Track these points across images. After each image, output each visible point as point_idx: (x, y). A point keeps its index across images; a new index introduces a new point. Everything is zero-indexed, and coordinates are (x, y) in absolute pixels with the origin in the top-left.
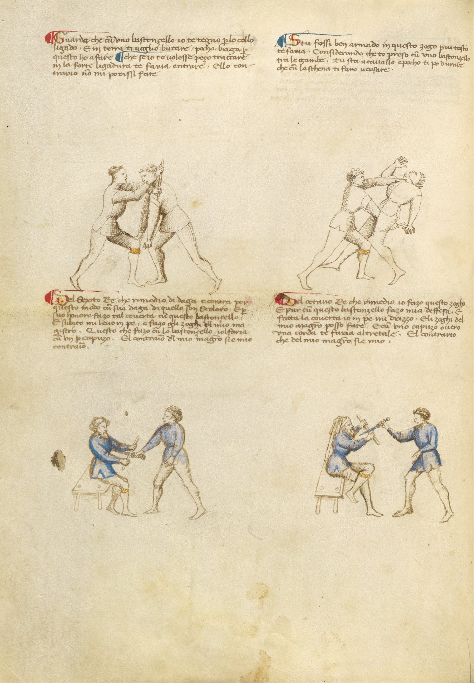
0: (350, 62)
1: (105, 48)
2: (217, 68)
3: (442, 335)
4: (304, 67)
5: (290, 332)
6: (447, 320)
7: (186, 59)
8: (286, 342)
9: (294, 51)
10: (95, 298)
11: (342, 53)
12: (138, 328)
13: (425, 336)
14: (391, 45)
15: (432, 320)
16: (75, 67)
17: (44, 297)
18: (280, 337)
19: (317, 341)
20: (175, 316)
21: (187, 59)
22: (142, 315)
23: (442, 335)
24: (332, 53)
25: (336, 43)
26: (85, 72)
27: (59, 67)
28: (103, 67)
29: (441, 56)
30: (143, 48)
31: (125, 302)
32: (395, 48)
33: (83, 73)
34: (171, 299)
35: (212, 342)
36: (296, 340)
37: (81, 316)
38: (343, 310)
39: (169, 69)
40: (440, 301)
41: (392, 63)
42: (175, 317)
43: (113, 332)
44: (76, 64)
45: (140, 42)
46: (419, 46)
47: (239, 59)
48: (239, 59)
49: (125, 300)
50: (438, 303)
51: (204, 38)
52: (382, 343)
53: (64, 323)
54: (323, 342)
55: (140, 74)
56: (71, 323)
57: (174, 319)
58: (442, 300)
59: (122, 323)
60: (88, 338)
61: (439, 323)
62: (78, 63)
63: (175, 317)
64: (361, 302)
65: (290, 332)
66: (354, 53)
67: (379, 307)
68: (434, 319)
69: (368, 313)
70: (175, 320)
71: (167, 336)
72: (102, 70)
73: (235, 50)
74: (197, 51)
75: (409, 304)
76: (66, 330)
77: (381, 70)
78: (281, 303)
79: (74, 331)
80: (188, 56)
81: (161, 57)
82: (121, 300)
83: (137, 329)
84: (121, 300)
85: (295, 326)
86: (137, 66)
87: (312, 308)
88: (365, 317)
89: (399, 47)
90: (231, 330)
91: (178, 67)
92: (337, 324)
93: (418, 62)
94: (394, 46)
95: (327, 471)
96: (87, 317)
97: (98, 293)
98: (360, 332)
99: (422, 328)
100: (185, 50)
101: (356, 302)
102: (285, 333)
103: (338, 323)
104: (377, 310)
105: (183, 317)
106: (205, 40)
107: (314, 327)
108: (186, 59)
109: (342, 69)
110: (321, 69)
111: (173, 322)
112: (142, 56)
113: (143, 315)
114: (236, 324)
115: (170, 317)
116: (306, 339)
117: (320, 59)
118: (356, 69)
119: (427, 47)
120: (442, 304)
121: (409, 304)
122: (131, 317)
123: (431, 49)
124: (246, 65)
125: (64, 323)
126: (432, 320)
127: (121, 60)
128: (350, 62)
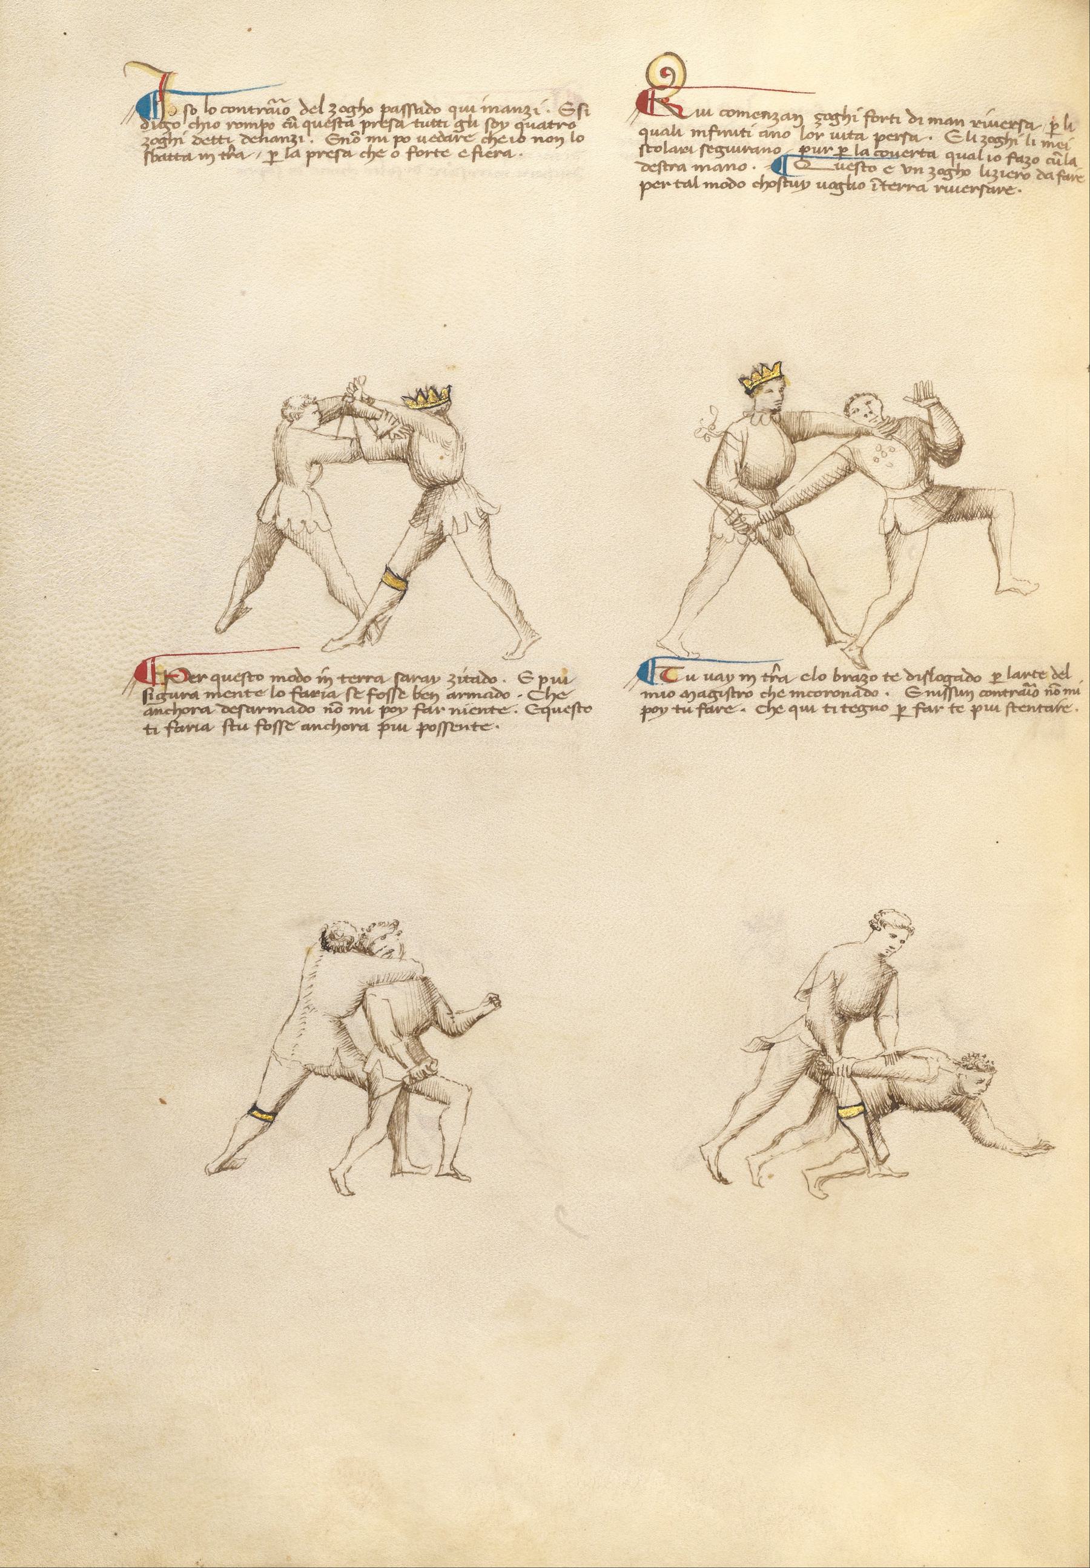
0: (228, 728)
2: (526, 683)
6: (170, 143)
8: (379, 156)
9: (382, 138)
10: (420, 121)
11: (477, 712)
12: (416, 148)
15: (975, 141)
16: (258, 730)
17: (635, 101)
20: (958, 155)
22: (909, 150)
25: (415, 694)
26: (329, 707)
27: (752, 679)
29: (155, 158)
33: (326, 709)
34: (914, 117)
35: (839, 192)
37: (810, 136)
42: (959, 157)
43: (258, 679)
50: (571, 710)
51: (856, 705)
55: (169, 728)
57: (957, 161)
58: (578, 703)
61: (991, 146)
63: (959, 157)
66: (421, 109)
68: (979, 139)
70: (959, 165)
79: (307, 679)
80: (285, 724)
83: (413, 149)
88: (768, 129)
89: (805, 712)
90: (262, 722)
91: (1029, 710)
92: (278, 724)
93: (654, 709)
102: (734, 165)
103: (281, 722)
105: (388, 124)
106: (859, 708)
107: (725, 152)
108: (281, 729)
110: (357, 680)
111: (955, 167)
114: (320, 127)
115: (947, 157)
120: (863, 171)
123: (866, 713)
124: (819, 187)
127: (649, 110)
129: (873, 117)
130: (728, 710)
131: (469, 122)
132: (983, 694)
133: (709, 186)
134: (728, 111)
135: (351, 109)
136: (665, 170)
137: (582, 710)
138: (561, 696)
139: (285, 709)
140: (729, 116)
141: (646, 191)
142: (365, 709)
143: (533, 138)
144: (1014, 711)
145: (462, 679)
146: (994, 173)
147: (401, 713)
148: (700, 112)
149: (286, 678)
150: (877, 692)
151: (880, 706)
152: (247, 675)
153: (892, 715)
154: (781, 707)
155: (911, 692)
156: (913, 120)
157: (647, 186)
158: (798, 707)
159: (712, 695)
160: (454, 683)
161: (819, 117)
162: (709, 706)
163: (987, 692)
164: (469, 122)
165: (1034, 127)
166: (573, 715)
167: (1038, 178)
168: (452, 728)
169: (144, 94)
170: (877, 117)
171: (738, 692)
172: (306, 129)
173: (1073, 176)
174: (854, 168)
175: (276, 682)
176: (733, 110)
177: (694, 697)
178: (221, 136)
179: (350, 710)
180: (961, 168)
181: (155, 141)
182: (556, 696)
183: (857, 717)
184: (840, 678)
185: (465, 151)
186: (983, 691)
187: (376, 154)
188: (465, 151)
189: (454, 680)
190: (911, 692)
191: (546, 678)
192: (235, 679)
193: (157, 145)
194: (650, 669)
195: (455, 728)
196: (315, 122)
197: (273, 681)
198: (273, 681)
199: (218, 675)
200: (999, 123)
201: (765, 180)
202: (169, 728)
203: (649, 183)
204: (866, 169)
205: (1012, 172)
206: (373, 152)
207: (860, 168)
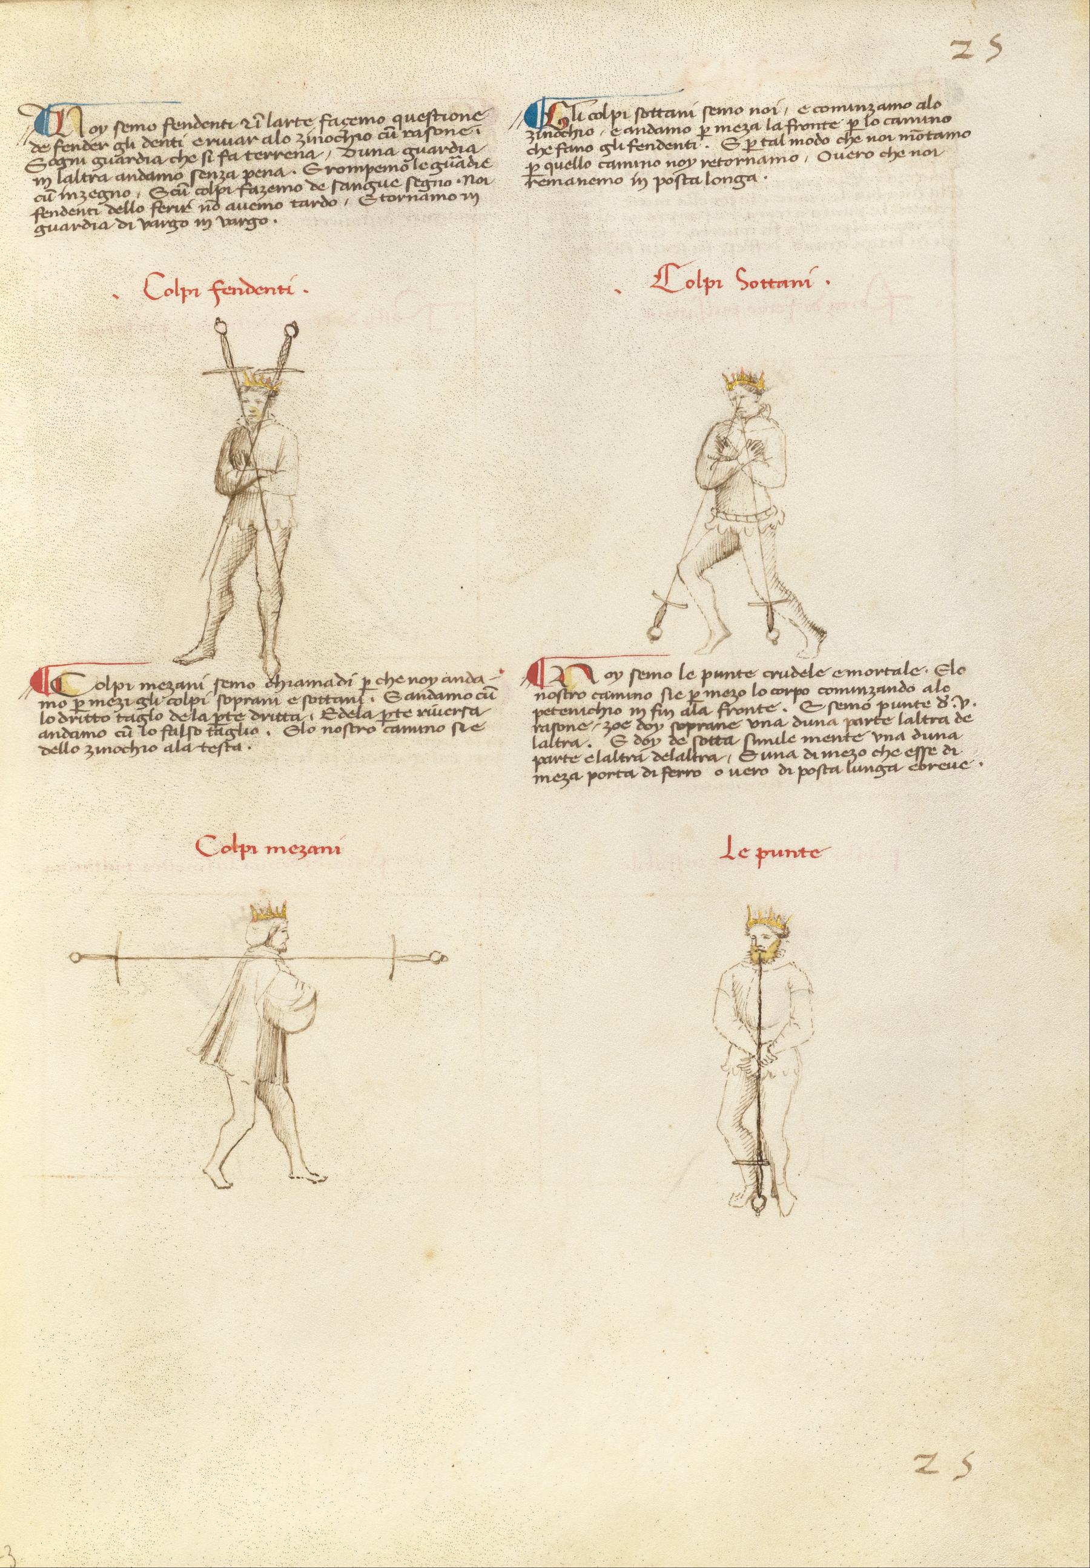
1: (763, 141)
4: (366, 710)
5: (391, 149)
13: (389, 200)
24: (207, 159)
28: (227, 734)
31: (888, 757)
32: (698, 701)
36: (152, 142)
39: (898, 772)
42: (557, 168)
44: (793, 123)
47: (129, 180)
48: (129, 180)
52: (682, 161)
53: (667, 696)
58: (435, 110)
62: (796, 121)
64: (971, 719)
65: (391, 149)
67: (581, 157)
69: (872, 695)
72: (420, 191)
74: (801, 775)
75: (653, 715)
77: (853, 690)
81: (746, 674)
86: (251, 157)
87: (576, 157)
95: (825, 161)
108: (575, 161)
109: (664, 773)
112: (708, 110)
113: (100, 144)
117: (645, 740)
121: (653, 715)
122: (829, 691)
123: (441, 170)
125: (667, 696)
126: (84, 163)
128: (167, 733)
129: (159, 208)
130: (239, 747)
131: (150, 700)
132: (775, 692)
136: (565, 698)
138: (895, 753)
140: (827, 694)
141: (660, 187)
142: (273, 698)
143: (40, 702)
145: (547, 760)
147: (617, 679)
149: (941, 119)
150: (808, 690)
153: (523, 176)
155: (391, 697)
157: (804, 772)
160: (874, 111)
161: (374, 185)
162: (568, 145)
163: (778, 690)
164: (150, 700)
168: (639, 675)
169: (532, 662)
171: (571, 693)
172: (549, 170)
175: (45, 709)
179: (536, 697)
182: (890, 754)
183: (876, 777)
184: (925, 766)
186: (774, 689)
187: (897, 155)
189: (91, 750)
190: (391, 697)
196: (544, 699)
197: (42, 707)
198: (42, 707)
199: (400, 116)
202: (630, 145)
203: (806, 770)
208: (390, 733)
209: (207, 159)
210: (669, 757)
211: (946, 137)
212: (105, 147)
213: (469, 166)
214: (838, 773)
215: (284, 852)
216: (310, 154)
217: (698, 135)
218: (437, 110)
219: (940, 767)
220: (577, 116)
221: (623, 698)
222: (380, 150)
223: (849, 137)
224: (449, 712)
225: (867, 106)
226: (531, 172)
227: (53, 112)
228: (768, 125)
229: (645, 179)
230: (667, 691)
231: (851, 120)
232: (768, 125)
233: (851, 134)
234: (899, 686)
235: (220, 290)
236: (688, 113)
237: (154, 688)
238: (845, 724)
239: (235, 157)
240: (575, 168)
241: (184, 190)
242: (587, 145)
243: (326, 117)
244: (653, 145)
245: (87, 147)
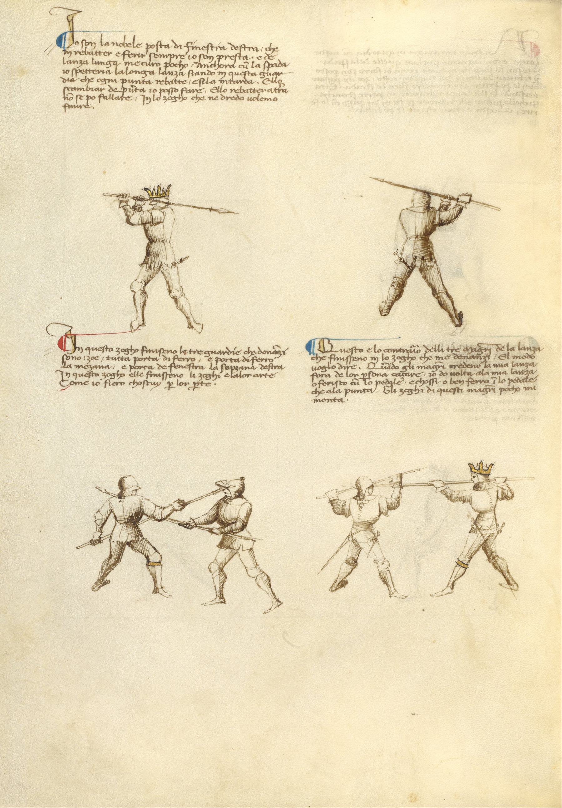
3: (221, 48)
7: (350, 362)
14: (84, 349)
16: (468, 384)
18: (315, 389)
19: (225, 91)
21: (352, 361)
23: (221, 48)
24: (202, 82)
30: (408, 390)
32: (76, 377)
38: (452, 382)
40: (144, 382)
41: (502, 382)
45: (346, 360)
46: (115, 350)
49: (273, 48)
53: (191, 75)
54: (157, 83)
56: (88, 89)
58: (355, 347)
59: (149, 98)
60: (527, 377)
71: (243, 356)
73: (210, 353)
76: (340, 382)
78: (63, 348)
81: (269, 376)
82: (178, 64)
84: (178, 64)
85: (325, 391)
92: (349, 358)
94: (88, 349)
96: (479, 383)
97: (102, 335)
98: (330, 390)
99: (232, 369)
100: (198, 353)
101: (427, 357)
103: (172, 88)
104: (274, 81)
115: (73, 375)
116: (252, 101)
118: (446, 373)
119: (125, 351)
125: (191, 75)
133: (471, 391)
134: (388, 350)
135: (112, 375)
136: (458, 392)
137: (94, 375)
139: (426, 367)
144: (93, 376)
146: (175, 73)
148: (314, 368)
151: (83, 382)
152: (457, 389)
154: (431, 357)
156: (223, 98)
158: (234, 73)
159: (143, 72)
165: (472, 374)
166: (76, 377)
167: (221, 99)
170: (132, 54)
171: (196, 366)
173: (193, 90)
174: (234, 58)
176: (390, 350)
177: (216, 377)
178: (255, 89)
180: (514, 388)
181: (109, 375)
185: (227, 374)
188: (227, 374)
191: (126, 80)
192: (450, 391)
193: (110, 377)
194: (63, 344)
195: (355, 359)
200: (84, 375)
201: (119, 373)
202: (468, 382)
204: (108, 350)
205: (115, 383)
206: (423, 381)
207: (210, 48)
208: (145, 66)
209: (202, 82)
210: (84, 53)
211: (244, 369)
212: (265, 91)
213: (279, 66)
214: (168, 48)
215: (200, 49)
216: (213, 82)
217: (155, 553)
218: (162, 42)
219: (231, 98)
220: (192, 375)
221: (153, 352)
222: (361, 358)
223: (181, 96)
224: (114, 384)
225: (78, 61)
226: (364, 377)
227: (214, 47)
228: (64, 62)
229: (377, 358)
230: (191, 72)
231: (135, 357)
232: (64, 62)
233: (182, 95)
234: (207, 72)
235: (247, 48)
236: (111, 81)
237: (500, 374)
238: (146, 46)
239: (97, 375)
240: (435, 351)
241: (247, 66)
242: (428, 365)
243: (322, 382)
244: (205, 73)
245: (529, 357)
